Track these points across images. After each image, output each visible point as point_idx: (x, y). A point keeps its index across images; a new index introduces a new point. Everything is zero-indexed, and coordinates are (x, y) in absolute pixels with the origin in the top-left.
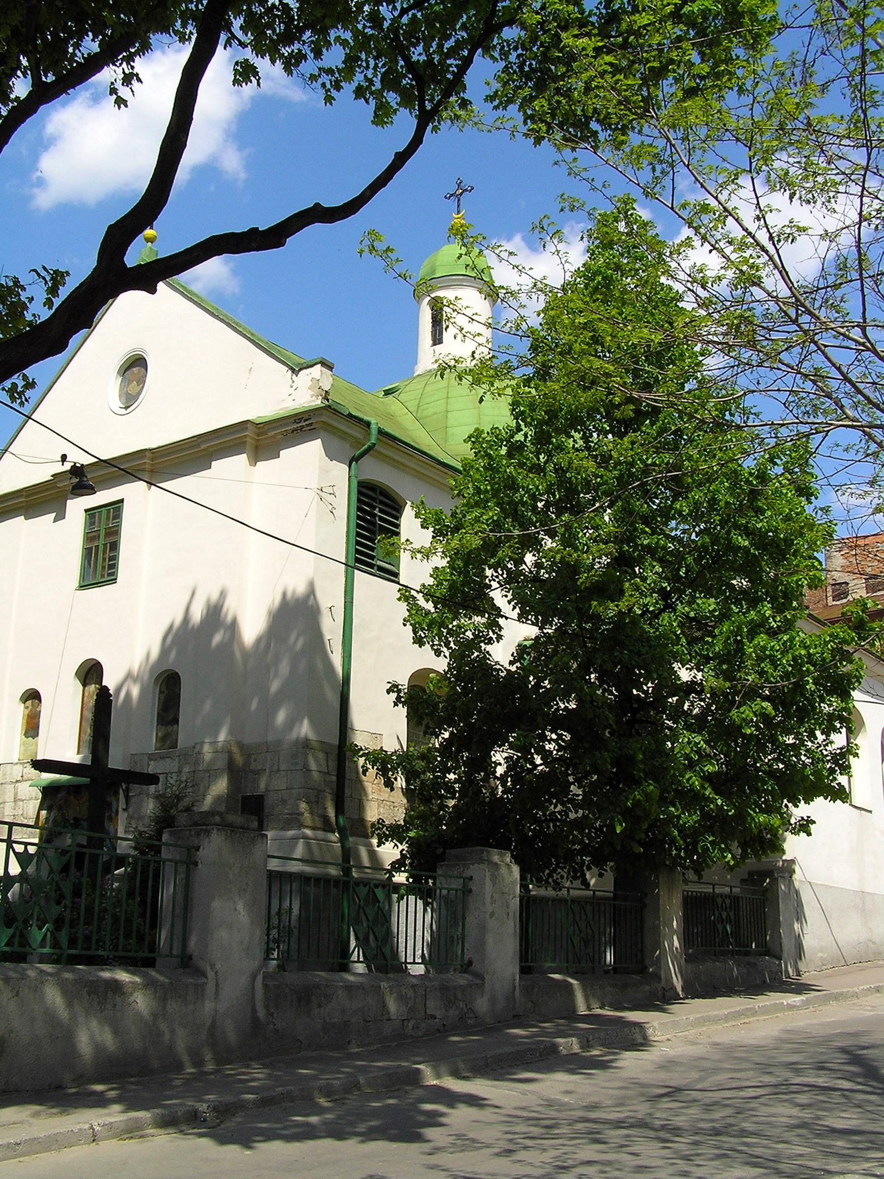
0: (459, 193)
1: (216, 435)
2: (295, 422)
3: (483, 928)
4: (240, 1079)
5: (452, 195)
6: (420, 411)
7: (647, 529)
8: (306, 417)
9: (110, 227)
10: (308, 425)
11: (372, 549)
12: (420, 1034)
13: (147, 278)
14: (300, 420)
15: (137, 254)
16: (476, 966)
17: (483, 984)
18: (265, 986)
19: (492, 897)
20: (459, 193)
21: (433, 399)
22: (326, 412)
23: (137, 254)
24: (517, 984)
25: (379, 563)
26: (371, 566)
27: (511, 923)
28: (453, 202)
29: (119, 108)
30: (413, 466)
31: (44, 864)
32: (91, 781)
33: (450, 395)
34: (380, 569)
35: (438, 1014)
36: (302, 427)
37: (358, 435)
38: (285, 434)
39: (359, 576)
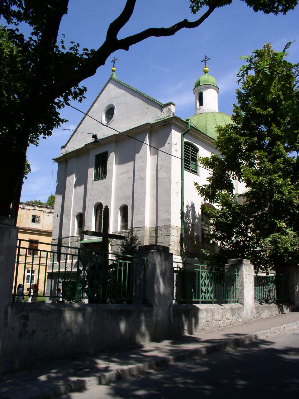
0: (206, 60)
1: (134, 130)
2: (164, 123)
3: (242, 286)
4: (246, 348)
5: (203, 61)
6: (198, 125)
7: (82, 291)
8: (167, 120)
9: (95, 73)
10: (168, 123)
11: (189, 164)
12: (225, 326)
13: (126, 44)
14: (166, 122)
15: (122, 35)
16: (240, 300)
17: (243, 307)
18: (174, 310)
19: (246, 276)
20: (206, 60)
21: (202, 121)
22: (174, 119)
23: (122, 35)
24: (254, 307)
25: (191, 169)
26: (189, 169)
27: (251, 285)
28: (204, 63)
29: (79, 102)
30: (201, 138)
31: (85, 272)
32: (103, 239)
33: (207, 120)
34: (192, 171)
35: (230, 318)
36: (166, 124)
37: (184, 127)
38: (161, 127)
39: (186, 173)
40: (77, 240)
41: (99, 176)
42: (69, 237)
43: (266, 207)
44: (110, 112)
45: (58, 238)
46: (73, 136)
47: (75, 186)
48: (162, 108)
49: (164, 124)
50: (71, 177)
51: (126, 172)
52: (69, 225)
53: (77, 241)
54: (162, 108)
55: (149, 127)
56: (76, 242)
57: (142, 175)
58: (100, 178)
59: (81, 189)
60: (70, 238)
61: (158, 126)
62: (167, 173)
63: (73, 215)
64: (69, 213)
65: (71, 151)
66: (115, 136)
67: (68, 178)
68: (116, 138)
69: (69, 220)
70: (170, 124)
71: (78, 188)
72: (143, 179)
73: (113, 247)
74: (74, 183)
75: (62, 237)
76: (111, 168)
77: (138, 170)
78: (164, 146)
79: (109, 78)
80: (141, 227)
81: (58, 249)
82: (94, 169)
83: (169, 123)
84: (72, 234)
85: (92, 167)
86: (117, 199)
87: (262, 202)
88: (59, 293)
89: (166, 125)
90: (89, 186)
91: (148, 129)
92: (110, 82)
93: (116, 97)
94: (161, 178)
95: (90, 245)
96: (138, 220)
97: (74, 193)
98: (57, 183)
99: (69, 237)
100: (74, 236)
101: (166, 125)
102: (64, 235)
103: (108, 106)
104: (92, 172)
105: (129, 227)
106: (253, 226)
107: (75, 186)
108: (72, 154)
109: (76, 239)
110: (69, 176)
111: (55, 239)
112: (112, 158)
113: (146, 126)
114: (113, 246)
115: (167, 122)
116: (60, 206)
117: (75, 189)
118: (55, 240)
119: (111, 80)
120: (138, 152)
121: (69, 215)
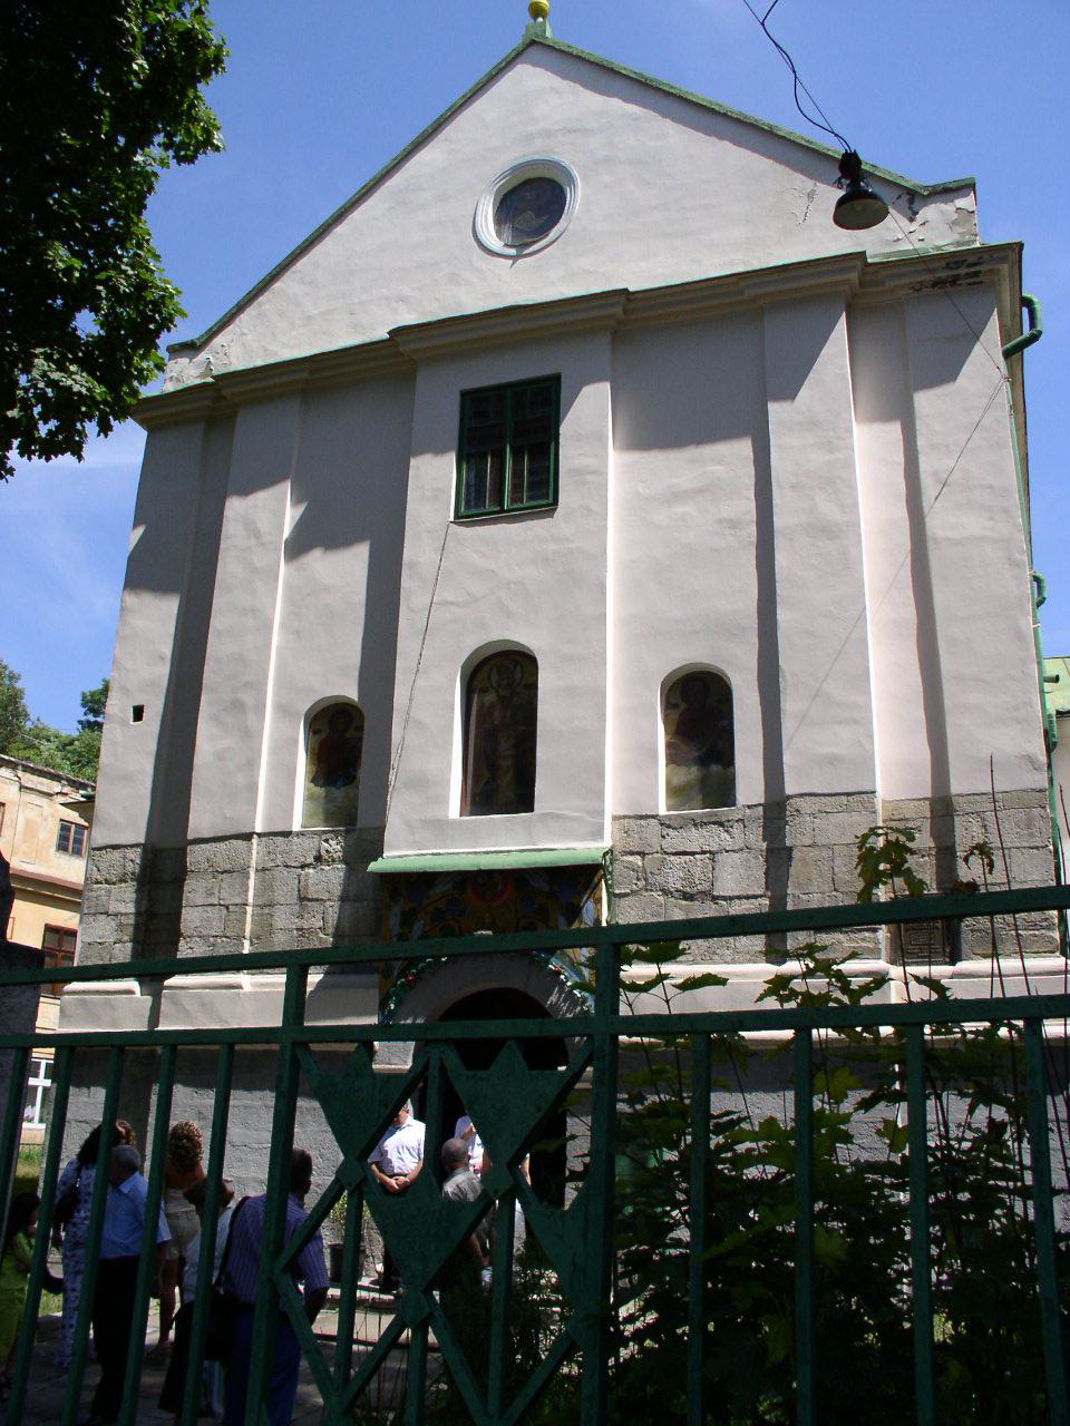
2: (947, 266)
8: (972, 259)
10: (968, 275)
14: (959, 264)
38: (918, 288)
40: (318, 858)
41: (501, 503)
42: (248, 837)
43: (673, 1146)
44: (533, 202)
45: (142, 841)
46: (261, 299)
47: (299, 546)
48: (911, 201)
49: (943, 274)
50: (261, 498)
51: (701, 491)
52: (252, 764)
53: (310, 860)
54: (911, 201)
55: (854, 276)
56: (303, 866)
57: (829, 510)
58: (502, 511)
59: (348, 568)
60: (255, 840)
61: (907, 280)
62: (991, 519)
63: (283, 710)
64: (248, 698)
65: (240, 367)
66: (622, 299)
67: (236, 508)
68: (625, 311)
69: (251, 736)
70: (981, 278)
71: (319, 562)
72: (837, 534)
73: (624, 902)
74: (286, 534)
75: (190, 837)
76: (588, 462)
77: (793, 487)
78: (955, 379)
79: (517, 42)
80: (848, 794)
81: (138, 902)
82: (450, 460)
83: (977, 274)
84: (268, 818)
85: (439, 450)
86: (644, 631)
87: (687, 1102)
88: (758, 942)
89: (954, 281)
90: (419, 549)
91: (846, 287)
92: (521, 58)
93: (570, 132)
94: (948, 539)
95: (441, 888)
96: (825, 750)
97: (288, 585)
98: (140, 531)
99: (248, 837)
100: (287, 834)
101: (954, 281)
102: (201, 819)
103: (515, 169)
104: (435, 477)
105: (749, 784)
106: (554, 1280)
107: (299, 546)
108: (187, 407)
109: (304, 849)
110: (246, 490)
111: (115, 847)
112: (590, 419)
113: (841, 271)
114: (616, 895)
115: (969, 266)
116: (162, 659)
117: (296, 563)
118: (117, 854)
119: (533, 47)
120: (789, 394)
121: (243, 710)
